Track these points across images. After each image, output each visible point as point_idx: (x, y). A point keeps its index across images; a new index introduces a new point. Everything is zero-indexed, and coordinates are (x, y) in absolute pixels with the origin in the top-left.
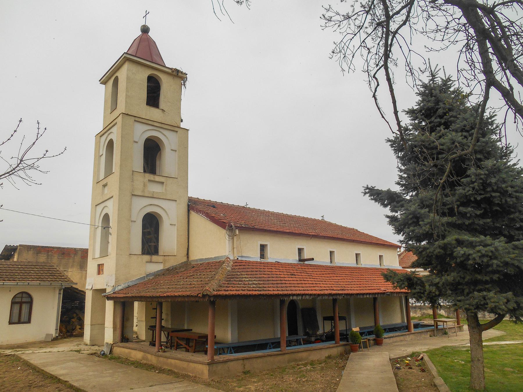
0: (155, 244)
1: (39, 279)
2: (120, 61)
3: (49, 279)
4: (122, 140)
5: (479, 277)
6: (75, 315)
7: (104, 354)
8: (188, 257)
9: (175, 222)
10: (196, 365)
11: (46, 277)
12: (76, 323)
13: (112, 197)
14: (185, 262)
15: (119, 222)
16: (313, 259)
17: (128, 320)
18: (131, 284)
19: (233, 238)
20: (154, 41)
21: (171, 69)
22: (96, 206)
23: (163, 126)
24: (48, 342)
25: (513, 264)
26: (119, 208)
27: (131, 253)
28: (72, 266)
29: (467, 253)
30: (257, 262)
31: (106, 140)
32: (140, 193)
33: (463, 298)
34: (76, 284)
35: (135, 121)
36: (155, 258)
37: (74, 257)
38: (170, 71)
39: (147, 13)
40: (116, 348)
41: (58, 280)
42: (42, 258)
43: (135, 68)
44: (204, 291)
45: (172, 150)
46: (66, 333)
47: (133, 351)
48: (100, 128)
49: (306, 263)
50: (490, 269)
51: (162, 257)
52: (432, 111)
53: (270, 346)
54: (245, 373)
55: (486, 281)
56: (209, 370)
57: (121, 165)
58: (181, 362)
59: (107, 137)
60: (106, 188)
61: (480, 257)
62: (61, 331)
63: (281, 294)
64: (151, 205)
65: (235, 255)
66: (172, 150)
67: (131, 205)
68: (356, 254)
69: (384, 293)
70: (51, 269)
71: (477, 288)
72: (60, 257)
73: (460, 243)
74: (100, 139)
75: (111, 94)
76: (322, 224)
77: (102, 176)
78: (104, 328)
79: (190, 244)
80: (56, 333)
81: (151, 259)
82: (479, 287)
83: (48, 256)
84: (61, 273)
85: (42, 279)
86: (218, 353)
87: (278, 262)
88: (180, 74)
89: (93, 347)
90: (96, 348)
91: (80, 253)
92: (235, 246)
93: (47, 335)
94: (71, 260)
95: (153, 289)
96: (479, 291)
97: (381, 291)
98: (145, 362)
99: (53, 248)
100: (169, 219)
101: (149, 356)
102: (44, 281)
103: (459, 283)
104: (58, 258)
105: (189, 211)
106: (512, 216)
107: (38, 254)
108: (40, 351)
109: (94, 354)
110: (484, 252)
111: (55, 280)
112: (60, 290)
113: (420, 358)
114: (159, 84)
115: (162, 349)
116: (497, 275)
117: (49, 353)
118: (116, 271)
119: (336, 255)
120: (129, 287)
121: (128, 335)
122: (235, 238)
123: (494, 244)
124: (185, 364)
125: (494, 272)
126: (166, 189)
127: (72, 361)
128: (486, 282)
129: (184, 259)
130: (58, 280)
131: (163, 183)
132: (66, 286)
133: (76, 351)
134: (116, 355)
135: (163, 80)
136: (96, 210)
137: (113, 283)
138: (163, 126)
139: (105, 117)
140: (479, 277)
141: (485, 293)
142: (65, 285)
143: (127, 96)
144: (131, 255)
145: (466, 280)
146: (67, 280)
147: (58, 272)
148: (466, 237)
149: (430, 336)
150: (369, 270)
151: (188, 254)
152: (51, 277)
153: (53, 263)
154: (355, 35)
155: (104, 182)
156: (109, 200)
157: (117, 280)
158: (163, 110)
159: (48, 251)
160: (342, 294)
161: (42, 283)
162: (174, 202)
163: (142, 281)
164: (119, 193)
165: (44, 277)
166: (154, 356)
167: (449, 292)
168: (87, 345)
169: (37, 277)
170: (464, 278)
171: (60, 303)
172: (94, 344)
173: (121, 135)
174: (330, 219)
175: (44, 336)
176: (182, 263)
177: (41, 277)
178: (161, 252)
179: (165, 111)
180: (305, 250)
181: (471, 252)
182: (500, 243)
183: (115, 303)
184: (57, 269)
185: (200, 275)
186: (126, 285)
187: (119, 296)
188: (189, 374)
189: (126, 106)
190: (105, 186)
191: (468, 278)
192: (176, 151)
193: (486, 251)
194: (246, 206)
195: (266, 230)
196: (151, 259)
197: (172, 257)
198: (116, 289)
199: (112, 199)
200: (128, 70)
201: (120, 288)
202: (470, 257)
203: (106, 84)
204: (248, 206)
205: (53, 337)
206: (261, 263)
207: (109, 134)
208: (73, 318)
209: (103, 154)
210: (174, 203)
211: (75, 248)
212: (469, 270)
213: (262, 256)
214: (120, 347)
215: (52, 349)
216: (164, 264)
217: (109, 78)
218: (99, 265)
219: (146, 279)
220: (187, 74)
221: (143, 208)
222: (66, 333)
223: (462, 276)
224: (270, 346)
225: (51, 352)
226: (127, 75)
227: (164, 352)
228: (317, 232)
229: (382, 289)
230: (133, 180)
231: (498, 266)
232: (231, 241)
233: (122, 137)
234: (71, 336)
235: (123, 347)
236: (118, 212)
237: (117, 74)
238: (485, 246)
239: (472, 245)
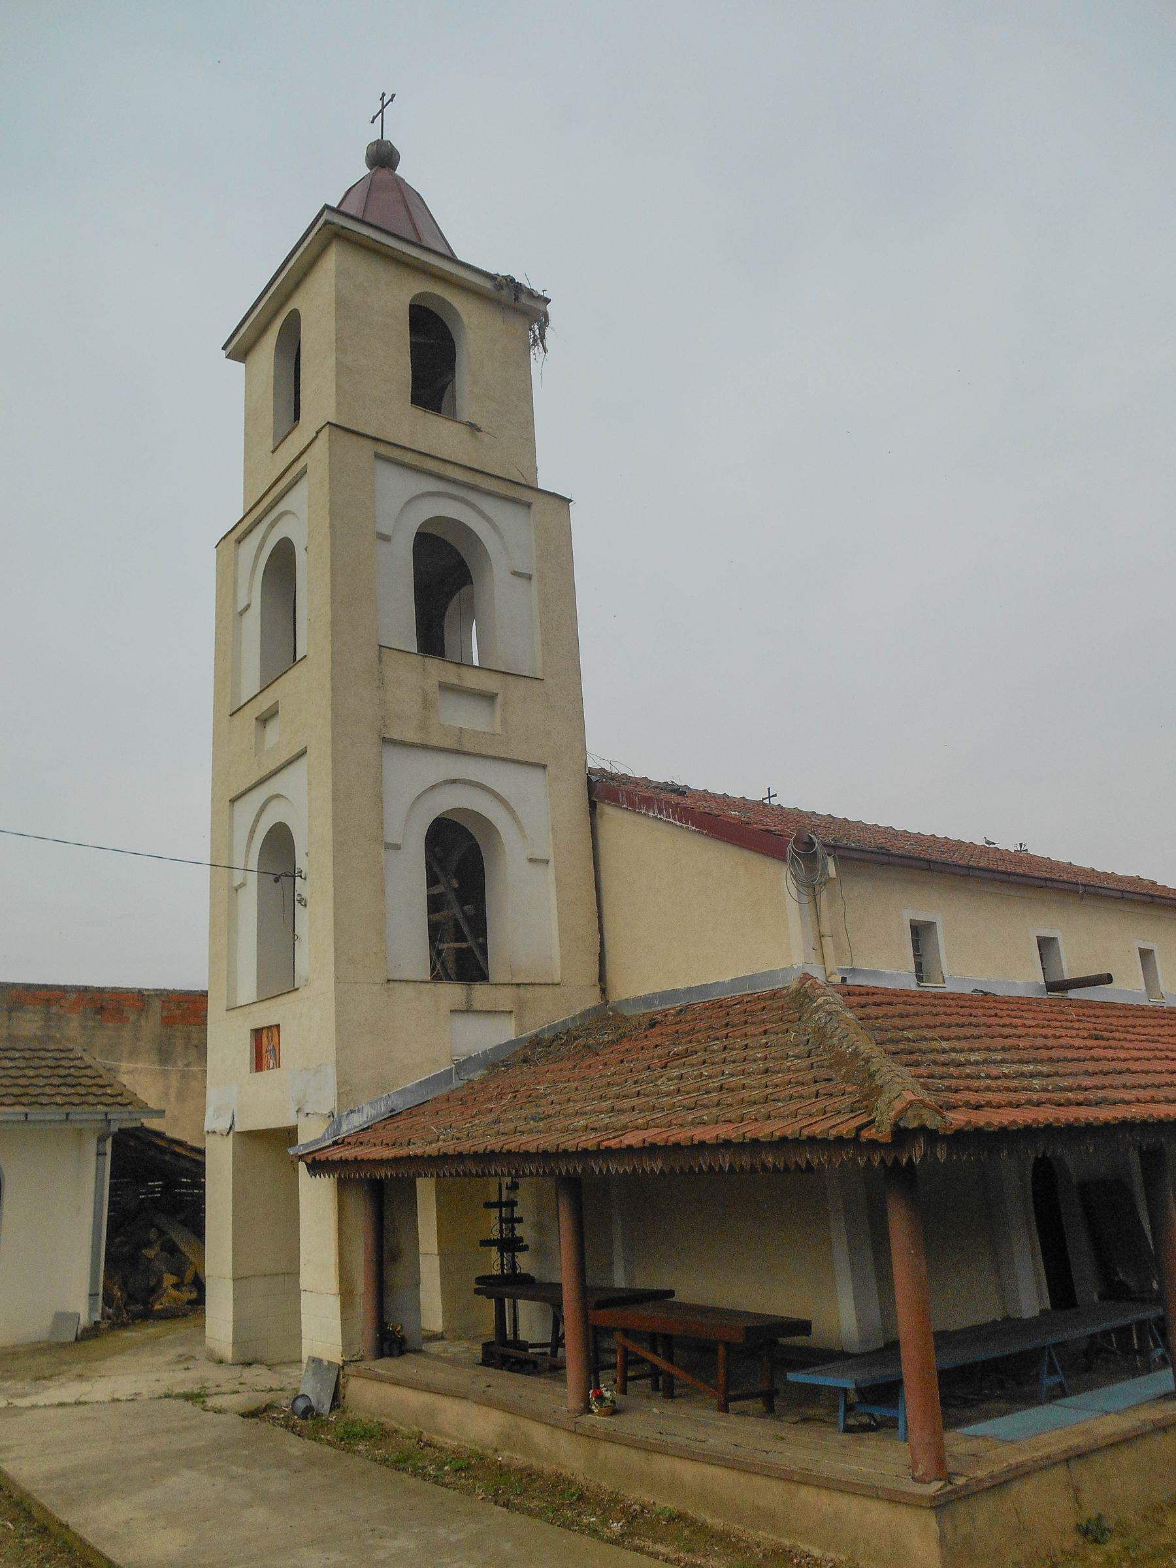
0: (464, 945)
1: (24, 1100)
2: (301, 249)
3: (58, 1099)
4: (332, 526)
6: (153, 1234)
7: (308, 1412)
8: (603, 991)
9: (548, 852)
10: (850, 1506)
11: (47, 1090)
12: (160, 1265)
13: (303, 753)
14: (594, 1009)
15: (340, 848)
16: (1108, 979)
17: (396, 1256)
18: (400, 1104)
19: (814, 897)
20: (418, 194)
21: (492, 278)
22: (233, 801)
23: (478, 480)
24: (64, 1346)
26: (335, 791)
27: (390, 977)
28: (133, 1054)
30: (907, 994)
31: (261, 547)
32: (411, 736)
34: (161, 1113)
35: (378, 456)
36: (481, 994)
37: (138, 1020)
38: (488, 285)
39: (385, 101)
40: (361, 1381)
41: (91, 1099)
42: (29, 1025)
43: (364, 269)
44: (905, 1110)
45: (515, 573)
46: (126, 1305)
47: (445, 1403)
48: (234, 511)
49: (1073, 994)
51: (507, 991)
53: (1051, 1364)
54: (1084, 1531)
56: (942, 1540)
57: (335, 623)
58: (744, 1479)
59: (264, 539)
60: (273, 728)
62: (108, 1300)
64: (454, 781)
65: (832, 966)
66: (515, 573)
67: (379, 781)
70: (63, 1063)
72: (90, 1023)
74: (237, 549)
75: (271, 380)
77: (251, 682)
78: (296, 1293)
79: (606, 934)
80: (92, 1309)
81: (469, 999)
83: (47, 1018)
84: (100, 1076)
85: (33, 1099)
86: (842, 1408)
87: (986, 994)
88: (524, 299)
89: (250, 1374)
90: (260, 1377)
91: (156, 1005)
92: (826, 928)
93: (61, 1318)
94: (127, 1034)
95: (533, 1119)
98: (520, 1459)
99: (64, 989)
100: (524, 837)
101: (539, 1434)
102: (42, 1104)
104: (84, 1027)
105: (592, 806)
107: (13, 1014)
108: (41, 1400)
109: (265, 1410)
111: (83, 1099)
112: (101, 1140)
114: (452, 341)
115: (600, 1398)
117: (75, 1409)
118: (340, 1049)
120: (394, 1116)
121: (398, 1322)
124: (770, 1494)
126: (504, 721)
127: (187, 1458)
129: (592, 999)
130: (91, 1099)
131: (490, 698)
132: (126, 1125)
133: (187, 1397)
134: (362, 1416)
135: (464, 317)
136: (231, 817)
137: (329, 1102)
138: (478, 480)
139: (248, 473)
142: (122, 1120)
143: (341, 369)
144: (392, 985)
146: (124, 1101)
147: (88, 1072)
151: (602, 978)
152: (64, 1090)
153: (68, 1040)
155: (264, 703)
156: (291, 768)
157: (345, 1089)
158: (473, 427)
159: (48, 1003)
161: (36, 1114)
162: (537, 773)
163: (445, 1090)
164: (333, 732)
165: (39, 1091)
166: (564, 1434)
168: (221, 1362)
169: (15, 1091)
171: (103, 1189)
172: (249, 1358)
173: (326, 510)
174: (1037, 849)
175: (48, 1321)
176: (584, 1014)
177: (31, 1090)
178: (497, 969)
179: (479, 430)
183: (343, 1185)
184: (86, 1059)
185: (725, 1048)
186: (383, 1108)
187: (371, 1157)
188: (804, 1547)
189: (339, 404)
190: (264, 720)
192: (529, 577)
194: (766, 801)
196: (469, 999)
197: (545, 990)
198: (344, 1128)
199: (302, 764)
200: (339, 273)
201: (358, 1121)
203: (252, 358)
204: (774, 802)
205: (81, 1327)
207: (272, 525)
208: (148, 1244)
209: (249, 605)
210: (534, 778)
211: (140, 990)
213: (920, 973)
214: (379, 1379)
215: (86, 1387)
216: (520, 1018)
217: (262, 330)
218: (257, 1033)
219: (456, 1084)
220: (548, 301)
221: (424, 792)
222: (126, 1305)
225: (85, 1403)
226: (338, 291)
227: (614, 1411)
230: (381, 681)
233: (332, 514)
234: (147, 1315)
235: (396, 1383)
236: (334, 807)
237: (295, 303)
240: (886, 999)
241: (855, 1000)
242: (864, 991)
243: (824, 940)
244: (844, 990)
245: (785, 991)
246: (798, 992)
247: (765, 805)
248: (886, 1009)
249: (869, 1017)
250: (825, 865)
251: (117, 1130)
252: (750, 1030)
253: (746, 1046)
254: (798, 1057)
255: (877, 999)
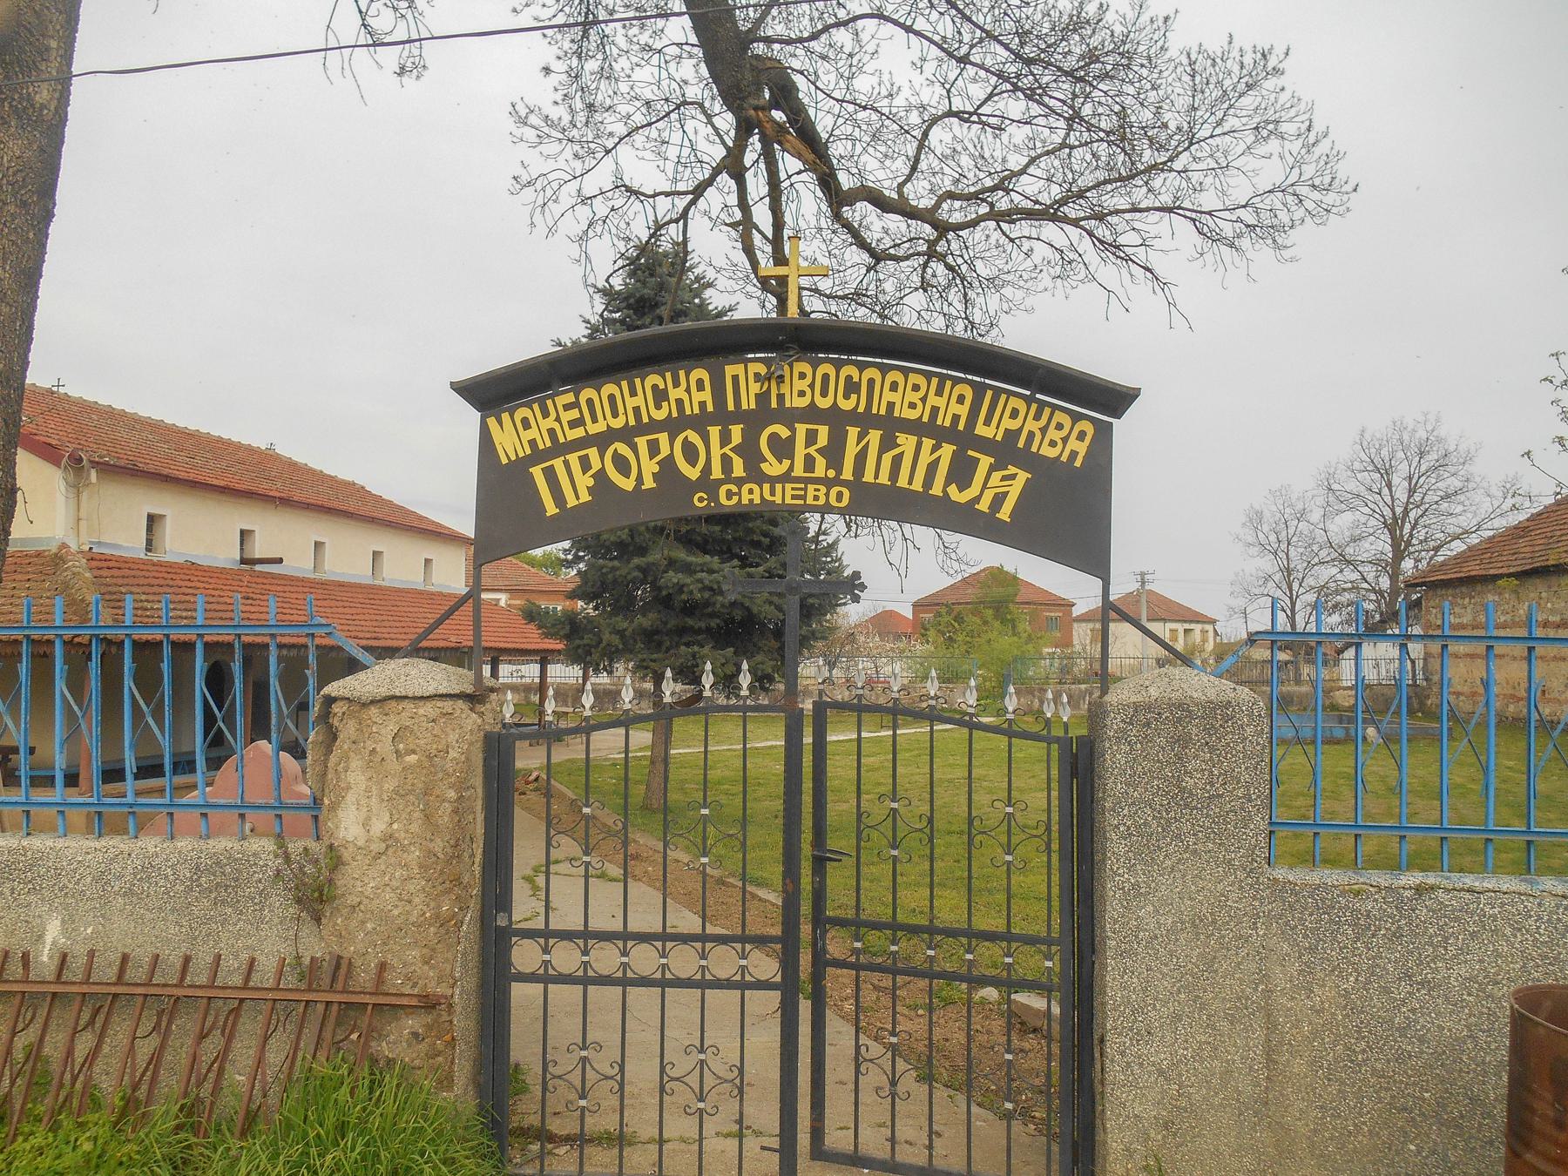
5: (690, 622)
16: (280, 561)
25: (742, 604)
29: (681, 582)
30: (134, 561)
33: (660, 655)
49: (258, 568)
50: (710, 609)
52: (648, 304)
53: (183, 768)
55: (700, 628)
61: (700, 590)
63: (258, 644)
65: (84, 538)
68: (243, 532)
69: (457, 649)
71: (683, 640)
73: (672, 563)
76: (265, 460)
82: (686, 639)
92: (83, 514)
96: (687, 645)
97: (453, 645)
103: (657, 632)
106: (750, 525)
110: (707, 582)
113: (532, 778)
116: (718, 621)
119: (328, 551)
122: (84, 496)
123: (723, 570)
125: (712, 615)
128: (699, 631)
140: (690, 622)
141: (696, 648)
145: (669, 626)
148: (681, 554)
149: (531, 745)
150: (404, 594)
154: (575, 178)
160: (378, 647)
167: (640, 645)
170: (666, 623)
180: (257, 535)
181: (688, 581)
182: (730, 569)
191: (672, 623)
193: (710, 581)
194: (55, 389)
195: (167, 476)
202: (685, 589)
204: (62, 390)
206: (144, 562)
212: (674, 610)
223: (664, 619)
224: (183, 768)
228: (351, 506)
229: (453, 639)
231: (723, 606)
232: (73, 502)
238: (711, 572)
239: (688, 569)
240: (117, 565)
241: (95, 564)
242: (103, 557)
243: (81, 522)
244: (89, 556)
245: (47, 553)
246: (56, 555)
247: (53, 393)
248: (115, 572)
249: (101, 577)
250: (89, 475)
251: (532, 626)
252: (18, 577)
253: (15, 588)
254: (48, 598)
255: (111, 564)
